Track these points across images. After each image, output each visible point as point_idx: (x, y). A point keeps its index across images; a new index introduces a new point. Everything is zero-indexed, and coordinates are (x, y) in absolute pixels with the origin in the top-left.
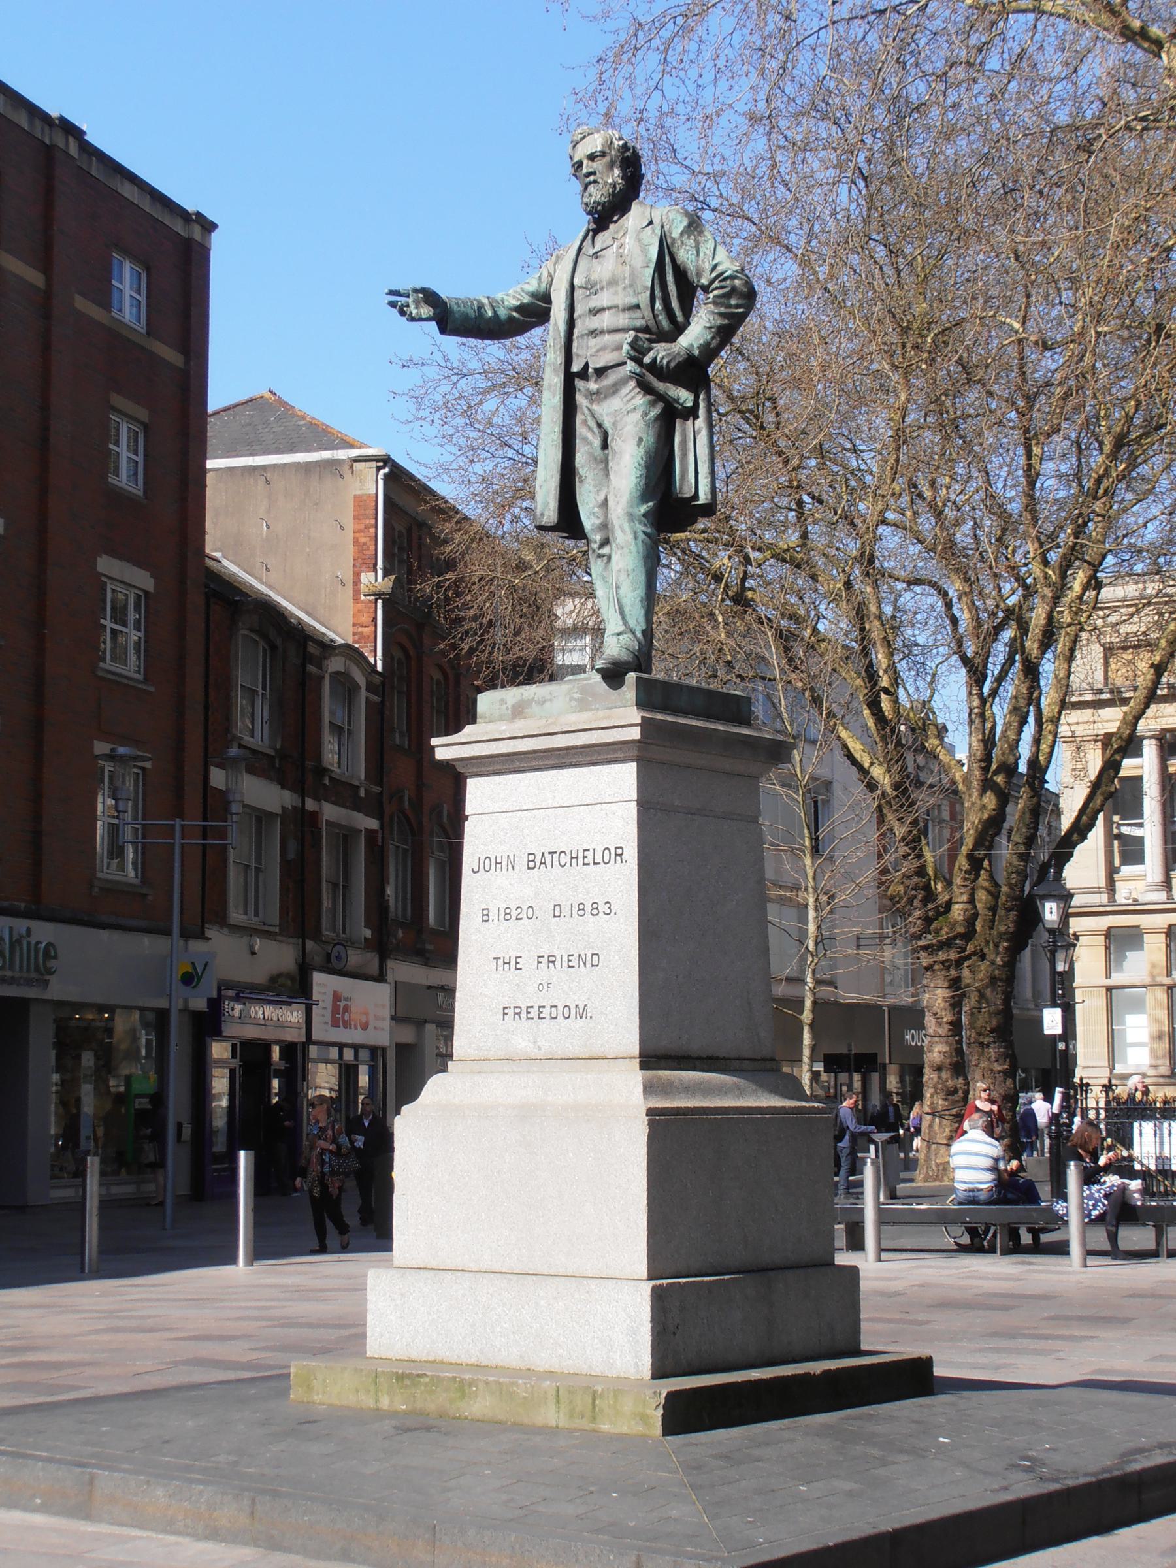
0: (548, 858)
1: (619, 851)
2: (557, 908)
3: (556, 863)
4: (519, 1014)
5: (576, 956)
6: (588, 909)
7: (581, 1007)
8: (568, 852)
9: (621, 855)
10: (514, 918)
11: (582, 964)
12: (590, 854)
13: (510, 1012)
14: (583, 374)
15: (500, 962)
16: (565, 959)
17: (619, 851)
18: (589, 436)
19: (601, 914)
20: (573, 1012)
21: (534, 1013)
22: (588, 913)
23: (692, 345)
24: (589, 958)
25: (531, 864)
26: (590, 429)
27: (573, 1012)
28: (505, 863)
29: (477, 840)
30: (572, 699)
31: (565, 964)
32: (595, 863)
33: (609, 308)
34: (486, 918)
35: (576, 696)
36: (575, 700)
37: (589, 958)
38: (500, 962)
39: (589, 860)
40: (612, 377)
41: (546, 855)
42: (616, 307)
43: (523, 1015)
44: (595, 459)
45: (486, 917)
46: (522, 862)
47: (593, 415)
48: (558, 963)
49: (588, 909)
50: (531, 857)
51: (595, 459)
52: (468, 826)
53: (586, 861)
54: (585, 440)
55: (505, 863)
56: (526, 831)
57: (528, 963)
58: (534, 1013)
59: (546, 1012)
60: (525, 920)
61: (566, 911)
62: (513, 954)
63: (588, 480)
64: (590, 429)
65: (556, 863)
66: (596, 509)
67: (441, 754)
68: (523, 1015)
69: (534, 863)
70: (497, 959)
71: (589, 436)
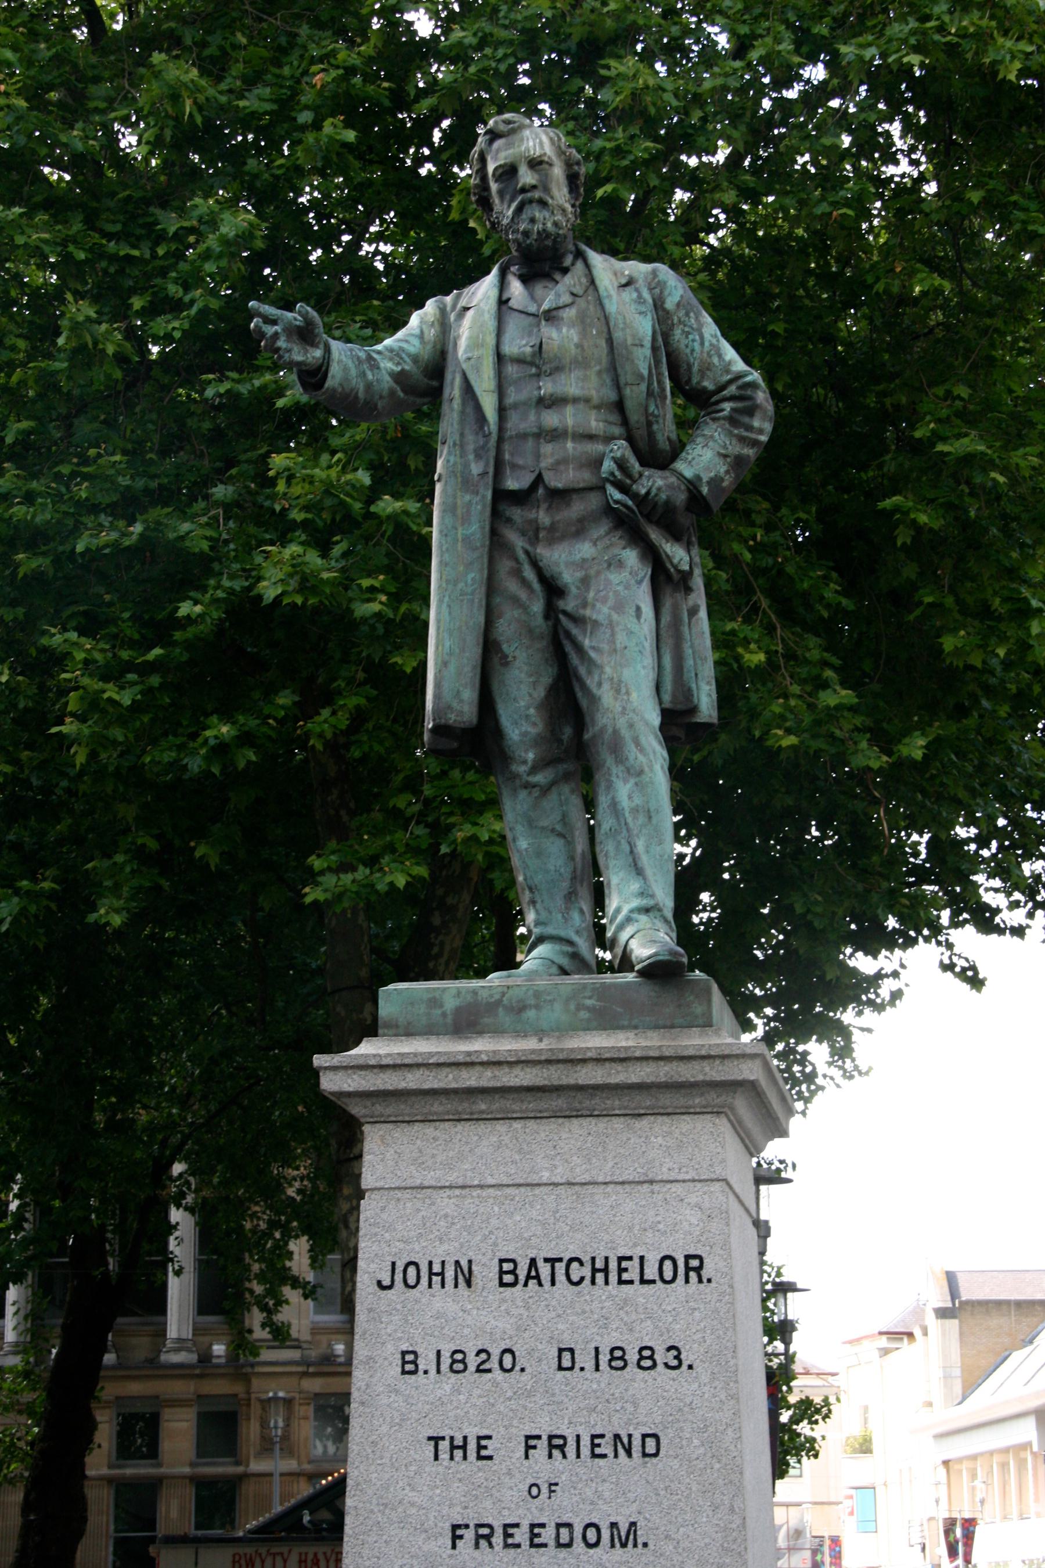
0: (545, 1270)
1: (694, 1263)
2: (566, 1356)
3: (560, 1276)
4: (488, 1538)
5: (609, 1436)
6: (632, 1356)
7: (624, 1529)
8: (586, 1259)
9: (698, 1270)
10: (472, 1368)
11: (621, 1451)
12: (633, 1266)
13: (469, 1535)
14: (521, 498)
15: (444, 1445)
16: (586, 1442)
17: (694, 1263)
18: (523, 595)
19: (660, 1367)
20: (606, 1534)
21: (521, 1536)
22: (472, 1368)
23: (699, 478)
24: (637, 1443)
25: (508, 1278)
26: (525, 583)
27: (606, 1534)
28: (450, 1274)
29: (384, 1231)
30: (579, 1007)
31: (585, 1451)
32: (643, 1281)
33: (575, 400)
34: (409, 1367)
35: (589, 1002)
36: (588, 1009)
37: (637, 1443)
38: (444, 1445)
39: (633, 1274)
40: (577, 508)
41: (540, 1264)
42: (587, 400)
43: (498, 1539)
44: (531, 631)
45: (409, 1363)
46: (486, 1273)
47: (535, 563)
48: (571, 1449)
49: (632, 1356)
50: (507, 1267)
51: (531, 631)
52: (368, 1208)
53: (625, 1276)
54: (516, 601)
55: (450, 1274)
56: (494, 1222)
57: (506, 1448)
58: (521, 1536)
59: (547, 1535)
60: (497, 1374)
61: (585, 1359)
62: (472, 1433)
63: (517, 663)
64: (525, 583)
65: (560, 1276)
66: (532, 711)
67: (329, 1083)
68: (498, 1539)
69: (508, 1275)
70: (436, 1440)
71: (523, 595)
